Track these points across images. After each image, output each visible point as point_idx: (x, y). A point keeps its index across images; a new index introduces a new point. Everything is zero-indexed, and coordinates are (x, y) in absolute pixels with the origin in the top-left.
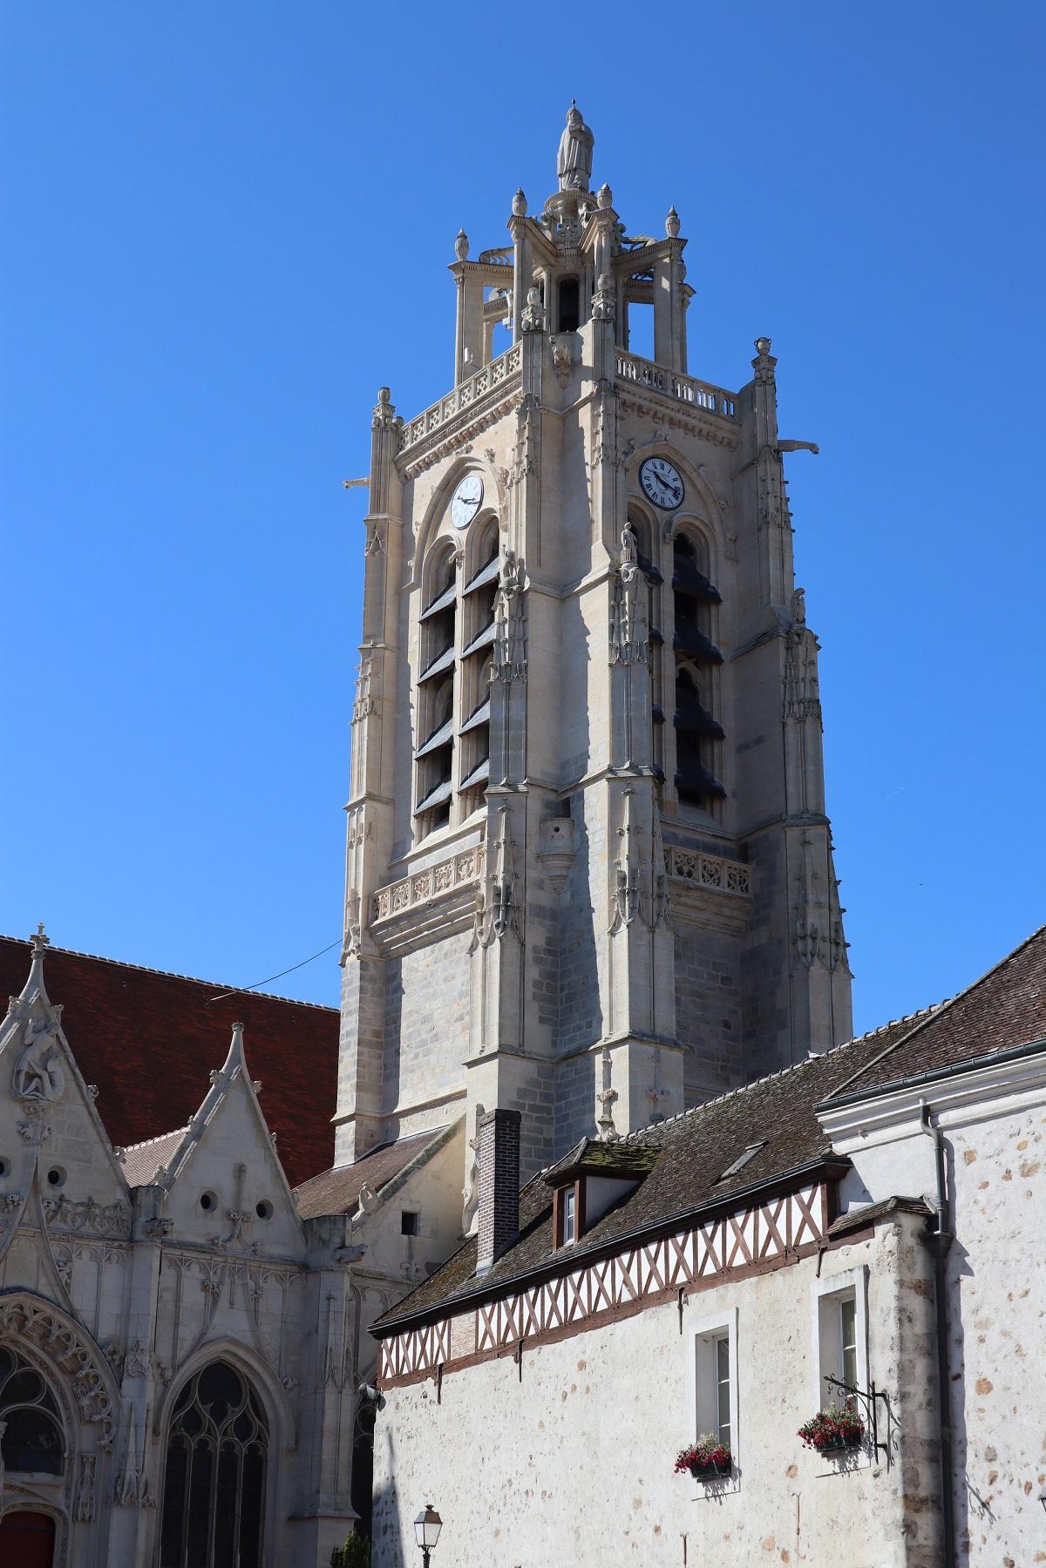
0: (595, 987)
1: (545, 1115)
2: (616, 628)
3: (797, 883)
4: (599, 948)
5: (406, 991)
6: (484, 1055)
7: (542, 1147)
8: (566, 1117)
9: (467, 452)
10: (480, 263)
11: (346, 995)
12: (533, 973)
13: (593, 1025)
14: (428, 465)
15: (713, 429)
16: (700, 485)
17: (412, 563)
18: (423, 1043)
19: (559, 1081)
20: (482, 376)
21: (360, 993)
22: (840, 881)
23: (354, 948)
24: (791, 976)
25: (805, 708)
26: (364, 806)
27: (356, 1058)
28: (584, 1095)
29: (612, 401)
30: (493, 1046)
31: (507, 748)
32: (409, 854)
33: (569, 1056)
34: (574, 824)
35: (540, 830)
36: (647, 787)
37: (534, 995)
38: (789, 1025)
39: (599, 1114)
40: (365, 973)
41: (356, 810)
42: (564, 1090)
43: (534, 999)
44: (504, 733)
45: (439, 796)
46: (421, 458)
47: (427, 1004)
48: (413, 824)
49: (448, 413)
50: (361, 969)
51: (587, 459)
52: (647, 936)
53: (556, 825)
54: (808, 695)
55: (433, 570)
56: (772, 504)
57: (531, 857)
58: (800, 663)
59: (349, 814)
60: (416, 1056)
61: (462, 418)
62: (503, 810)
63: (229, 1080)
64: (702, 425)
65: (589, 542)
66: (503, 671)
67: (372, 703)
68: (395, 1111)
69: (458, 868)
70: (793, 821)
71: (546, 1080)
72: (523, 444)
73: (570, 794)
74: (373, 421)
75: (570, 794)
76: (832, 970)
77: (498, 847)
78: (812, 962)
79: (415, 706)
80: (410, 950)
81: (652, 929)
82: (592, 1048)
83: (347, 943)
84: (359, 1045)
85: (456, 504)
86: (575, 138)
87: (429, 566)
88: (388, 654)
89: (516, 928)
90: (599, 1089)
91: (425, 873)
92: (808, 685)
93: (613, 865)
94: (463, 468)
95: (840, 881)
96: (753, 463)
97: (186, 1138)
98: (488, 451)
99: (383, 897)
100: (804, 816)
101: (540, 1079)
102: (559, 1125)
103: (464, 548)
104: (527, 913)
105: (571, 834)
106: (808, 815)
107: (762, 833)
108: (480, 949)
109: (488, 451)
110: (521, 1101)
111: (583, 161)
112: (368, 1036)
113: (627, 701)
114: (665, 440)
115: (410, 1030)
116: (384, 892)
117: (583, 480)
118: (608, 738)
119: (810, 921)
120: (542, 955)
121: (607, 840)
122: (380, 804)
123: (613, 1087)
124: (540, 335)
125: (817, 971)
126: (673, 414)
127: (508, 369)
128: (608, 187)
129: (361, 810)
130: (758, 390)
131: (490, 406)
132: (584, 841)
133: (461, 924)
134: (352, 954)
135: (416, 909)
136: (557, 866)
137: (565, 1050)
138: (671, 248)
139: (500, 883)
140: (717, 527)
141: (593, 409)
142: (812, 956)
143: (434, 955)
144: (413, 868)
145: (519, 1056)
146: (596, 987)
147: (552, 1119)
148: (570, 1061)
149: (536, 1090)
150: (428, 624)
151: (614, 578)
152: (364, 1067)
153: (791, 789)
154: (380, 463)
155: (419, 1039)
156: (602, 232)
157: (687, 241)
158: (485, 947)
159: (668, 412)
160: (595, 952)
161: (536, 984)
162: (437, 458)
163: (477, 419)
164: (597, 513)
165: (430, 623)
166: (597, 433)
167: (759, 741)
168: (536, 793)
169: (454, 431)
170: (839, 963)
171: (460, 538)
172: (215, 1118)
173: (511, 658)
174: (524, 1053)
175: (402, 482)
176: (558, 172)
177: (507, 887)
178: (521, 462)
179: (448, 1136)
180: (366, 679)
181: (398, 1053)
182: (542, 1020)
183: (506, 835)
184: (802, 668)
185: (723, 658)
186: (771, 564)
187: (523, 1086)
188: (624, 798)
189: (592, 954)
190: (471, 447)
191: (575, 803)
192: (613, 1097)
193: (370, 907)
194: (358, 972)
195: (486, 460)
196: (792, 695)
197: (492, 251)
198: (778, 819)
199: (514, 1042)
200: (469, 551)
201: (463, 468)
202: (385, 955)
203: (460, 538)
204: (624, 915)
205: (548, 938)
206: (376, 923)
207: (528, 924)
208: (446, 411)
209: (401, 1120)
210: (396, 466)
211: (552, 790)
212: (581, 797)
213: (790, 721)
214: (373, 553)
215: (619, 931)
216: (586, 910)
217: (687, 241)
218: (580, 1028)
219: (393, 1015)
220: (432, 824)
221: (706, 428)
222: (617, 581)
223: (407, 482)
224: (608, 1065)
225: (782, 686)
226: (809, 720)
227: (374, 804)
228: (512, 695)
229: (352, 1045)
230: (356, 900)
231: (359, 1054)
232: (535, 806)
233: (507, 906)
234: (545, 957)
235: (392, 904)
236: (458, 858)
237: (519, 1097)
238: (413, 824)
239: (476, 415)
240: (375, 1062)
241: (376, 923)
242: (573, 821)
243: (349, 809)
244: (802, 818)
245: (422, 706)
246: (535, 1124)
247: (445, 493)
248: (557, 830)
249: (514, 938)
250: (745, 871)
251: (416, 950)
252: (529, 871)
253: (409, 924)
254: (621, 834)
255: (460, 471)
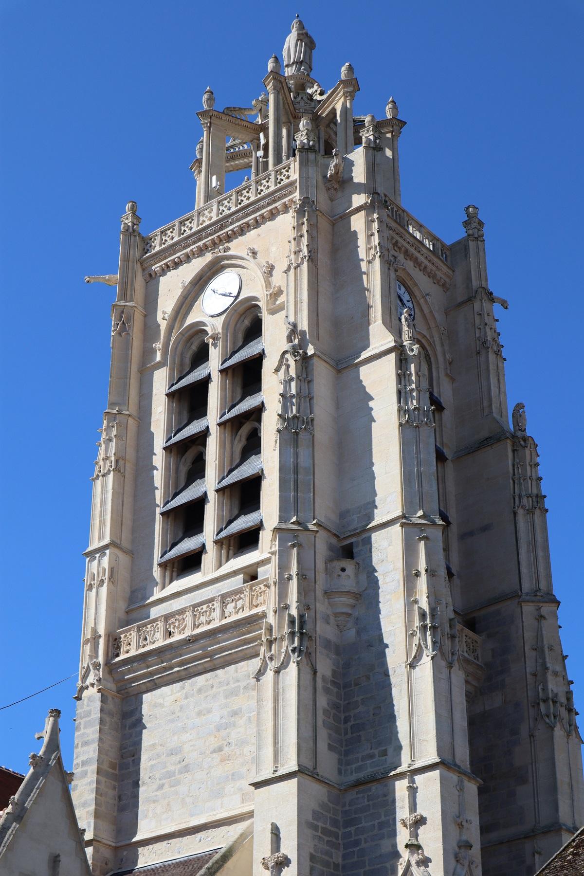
0: (392, 718)
1: (334, 840)
2: (403, 394)
3: (534, 653)
6: (278, 774)
7: (332, 871)
8: (357, 843)
9: (225, 252)
10: (223, 113)
11: (82, 726)
12: (323, 701)
14: (177, 265)
16: (426, 311)
17: (158, 345)
18: (170, 774)
19: (347, 808)
20: (244, 189)
21: (100, 724)
22: (567, 656)
23: (95, 681)
24: (532, 736)
25: (532, 501)
26: (107, 552)
27: (95, 785)
28: (380, 821)
29: (385, 213)
30: (291, 765)
33: (358, 784)
35: (326, 569)
36: (437, 534)
38: (530, 779)
39: (403, 836)
40: (105, 706)
41: (97, 556)
42: (353, 816)
44: (292, 476)
45: (188, 545)
47: (176, 738)
48: (157, 572)
49: (185, 231)
51: (362, 253)
52: (445, 671)
53: (342, 566)
54: (535, 491)
55: (178, 352)
56: (490, 335)
58: (528, 464)
59: (88, 559)
60: (161, 787)
61: (221, 223)
62: (293, 546)
63: (48, 765)
65: (366, 321)
67: (117, 461)
68: (134, 840)
70: (528, 598)
71: (334, 806)
72: (301, 236)
73: (353, 540)
75: (353, 540)
76: (569, 734)
77: (290, 578)
80: (155, 686)
81: (450, 666)
82: (393, 773)
83: (85, 676)
84: (98, 773)
85: (208, 294)
86: (301, 40)
87: (175, 348)
88: (131, 421)
89: (308, 655)
90: (402, 812)
91: (182, 612)
92: (534, 483)
93: (411, 602)
95: (567, 656)
96: (470, 300)
97: (7, 818)
98: (250, 249)
99: (125, 636)
100: (538, 594)
101: (329, 804)
102: (348, 851)
105: (357, 575)
107: (493, 609)
109: (250, 249)
110: (316, 822)
111: (307, 57)
112: (105, 767)
114: (402, 265)
115: (152, 763)
117: (358, 274)
121: (402, 579)
122: (120, 552)
123: (421, 811)
125: (559, 733)
128: (350, 65)
129: (104, 554)
130: (472, 245)
131: (253, 212)
132: (374, 584)
133: (222, 660)
134: (90, 688)
135: (171, 644)
136: (343, 603)
137: (354, 777)
138: (392, 127)
139: (294, 612)
141: (367, 215)
142: (555, 717)
143: (185, 691)
144: (155, 612)
147: (339, 844)
148: (361, 788)
149: (327, 814)
150: (174, 397)
151: (399, 352)
152: (101, 795)
153: (524, 570)
154: (128, 261)
156: (347, 97)
157: (406, 123)
158: (277, 672)
159: (405, 244)
160: (390, 685)
162: (188, 258)
166: (372, 235)
167: (485, 528)
171: (215, 326)
172: (35, 802)
173: (298, 411)
174: (318, 775)
175: (145, 280)
176: (286, 63)
177: (301, 616)
179: (226, 857)
180: (110, 440)
181: (136, 784)
182: (331, 748)
183: (298, 568)
184: (528, 468)
185: (447, 457)
187: (317, 809)
188: (418, 543)
189: (385, 685)
190: (229, 249)
191: (360, 548)
192: (420, 822)
193: (110, 645)
194: (98, 704)
195: (249, 257)
196: (520, 489)
197: (234, 108)
199: (309, 765)
200: (225, 334)
202: (123, 692)
203: (215, 326)
205: (333, 670)
206: (117, 659)
208: (201, 219)
209: (140, 849)
211: (335, 535)
212: (368, 542)
213: (520, 512)
214: (120, 334)
215: (419, 664)
216: (378, 646)
217: (406, 123)
218: (371, 756)
220: (231, 552)
221: (430, 266)
222: (401, 354)
223: (152, 279)
224: (413, 791)
225: (511, 481)
226: (537, 512)
230: (96, 637)
231: (98, 782)
232: (322, 544)
233: (302, 634)
234: (332, 688)
237: (314, 819)
238: (157, 572)
239: (238, 220)
240: (111, 793)
241: (117, 659)
242: (358, 564)
244: (536, 595)
245: (167, 468)
246: (326, 847)
248: (343, 570)
250: (476, 641)
251: (160, 687)
253: (159, 660)
254: (418, 575)
255: (214, 269)
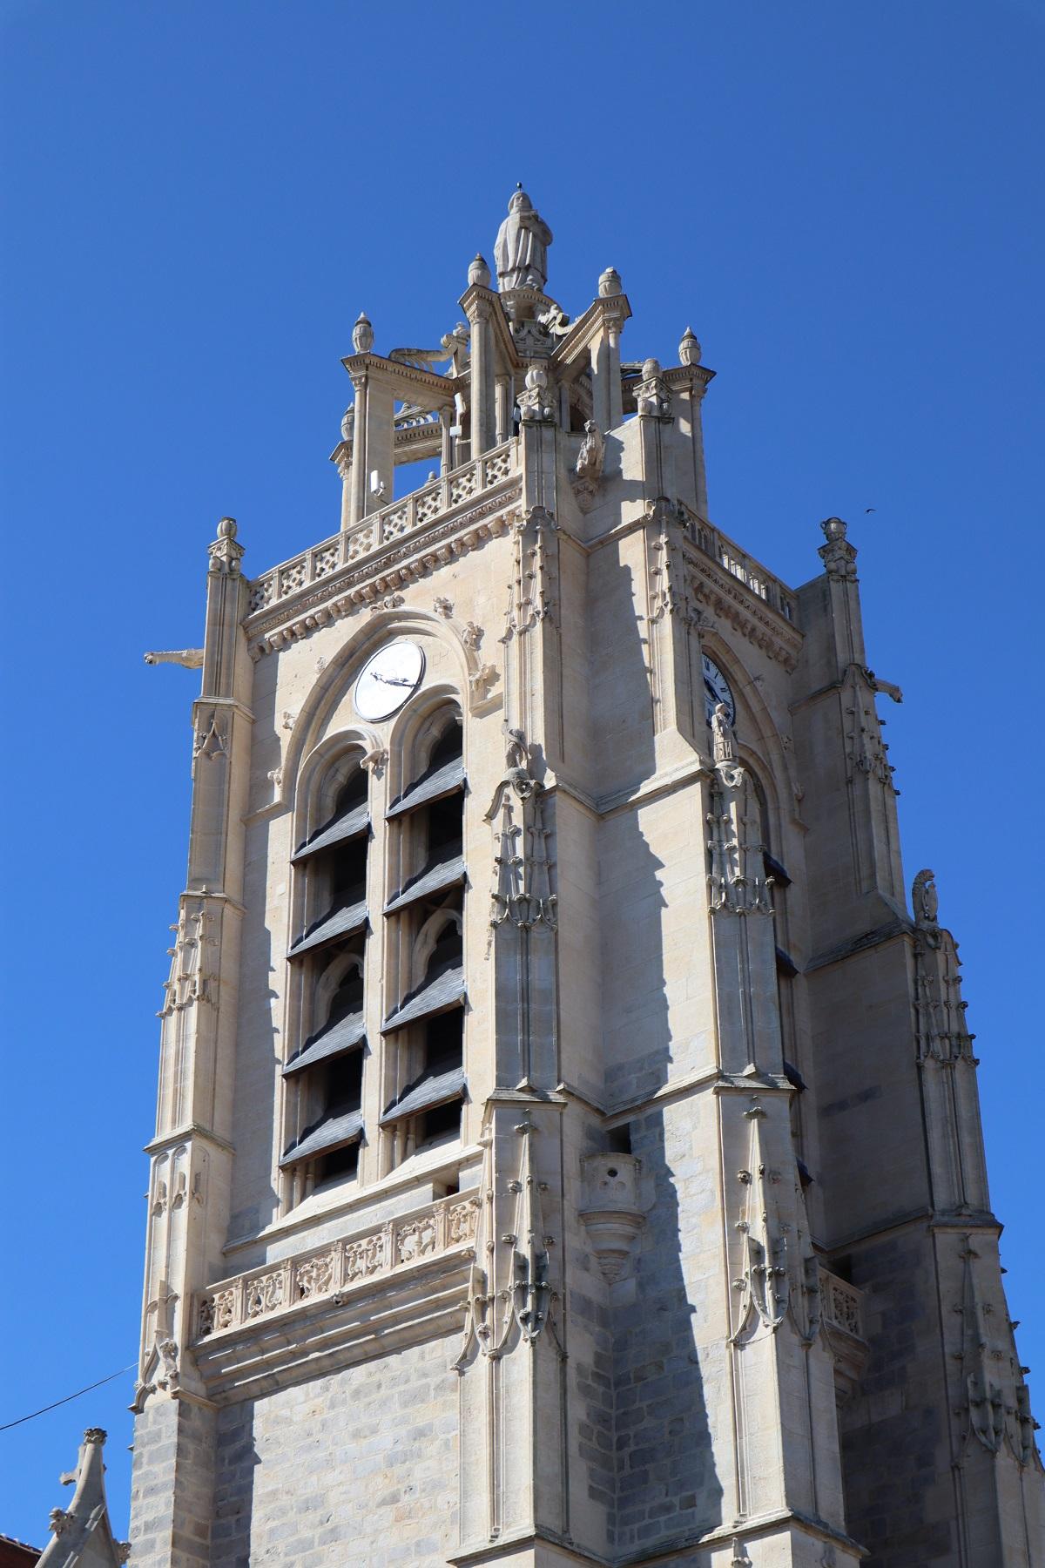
2: (716, 857)
3: (957, 1319)
4: (706, 1369)
5: (262, 1458)
6: (500, 1542)
9: (394, 606)
10: (389, 359)
12: (578, 1411)
13: (698, 1502)
14: (308, 630)
15: (768, 632)
16: (756, 708)
21: (178, 1456)
22: (1017, 1323)
23: (168, 1378)
25: (951, 1045)
26: (189, 1145)
29: (680, 532)
31: (526, 1030)
32: (269, 1230)
34: (640, 1169)
37: (581, 1446)
38: (955, 1547)
40: (186, 1423)
41: (170, 1152)
43: (581, 1455)
44: (520, 1006)
45: (334, 1131)
46: (405, 563)
47: (314, 1478)
48: (277, 1182)
50: (180, 1415)
51: (640, 606)
52: (799, 1353)
54: (955, 1028)
55: (313, 786)
56: (870, 749)
57: (570, 1215)
58: (941, 978)
59: (153, 1159)
61: (388, 555)
62: (523, 1131)
63: (84, 1530)
64: (755, 621)
65: (648, 728)
66: (517, 910)
67: (204, 983)
69: (398, 1237)
70: (946, 1219)
72: (531, 577)
73: (630, 1119)
74: (211, 562)
75: (630, 1119)
76: (1022, 1464)
77: (517, 1188)
78: (998, 1443)
79: (281, 993)
80: (275, 1386)
81: (807, 1343)
82: (706, 1538)
83: (150, 1370)
86: (526, 228)
87: (307, 780)
88: (229, 911)
89: (552, 1326)
91: (323, 1252)
92: (953, 1013)
93: (735, 1229)
94: (383, 631)
95: (1017, 1323)
96: (834, 686)
103: (388, 747)
104: (568, 1306)
106: (969, 1212)
107: (884, 1239)
108: (482, 1363)
112: (188, 1532)
113: (743, 970)
115: (272, 1524)
116: (230, 1285)
118: (712, 1027)
119: (989, 1377)
120: (589, 1382)
124: (553, 429)
126: (722, 593)
127: (484, 481)
130: (835, 588)
131: (445, 535)
132: (668, 1198)
133: (396, 1337)
134: (159, 1391)
136: (613, 1233)
138: (691, 380)
139: (525, 1250)
140: (778, 773)
141: (649, 538)
143: (329, 1395)
144: (276, 1253)
145: (564, 1548)
146: (704, 1438)
153: (937, 1169)
155: (292, 1539)
156: (609, 328)
157: (715, 373)
158: (496, 1358)
159: (716, 589)
160: (699, 1379)
161: (583, 1428)
162: (329, 619)
163: (417, 556)
164: (665, 686)
165: (309, 866)
166: (658, 572)
167: (866, 1096)
168: (574, 1109)
169: (369, 576)
170: (1029, 1452)
171: (376, 740)
173: (529, 888)
175: (253, 658)
177: (538, 1258)
178: (529, 603)
180: (192, 945)
182: (593, 1493)
183: (532, 1171)
184: (943, 986)
186: (874, 831)
193: (195, 1313)
194: (173, 1420)
196: (929, 1024)
198: (922, 1215)
199: (554, 1523)
200: (397, 754)
201: (383, 631)
202: (218, 1397)
203: (376, 740)
204: (764, 1311)
206: (207, 1339)
207: (569, 1324)
208: (352, 548)
210: (246, 632)
211: (597, 1110)
212: (657, 1122)
213: (929, 1064)
214: (208, 755)
215: (751, 1340)
216: (678, 1310)
217: (715, 373)
218: (668, 1508)
219: (234, 1499)
220: (411, 1144)
222: (712, 785)
223: (264, 657)
225: (912, 1011)
226: (960, 1064)
227: (205, 1144)
228: (532, 945)
229: (158, 1546)
230: (169, 1299)
232: (574, 1128)
233: (539, 1289)
235: (245, 1306)
236: (398, 1224)
238: (277, 1182)
239: (417, 550)
241: (207, 1339)
243: (152, 1151)
244: (960, 1215)
245: (295, 995)
247: (345, 670)
248: (613, 1173)
249: (550, 1344)
252: (568, 1236)
254: (746, 1180)
255: (376, 637)
